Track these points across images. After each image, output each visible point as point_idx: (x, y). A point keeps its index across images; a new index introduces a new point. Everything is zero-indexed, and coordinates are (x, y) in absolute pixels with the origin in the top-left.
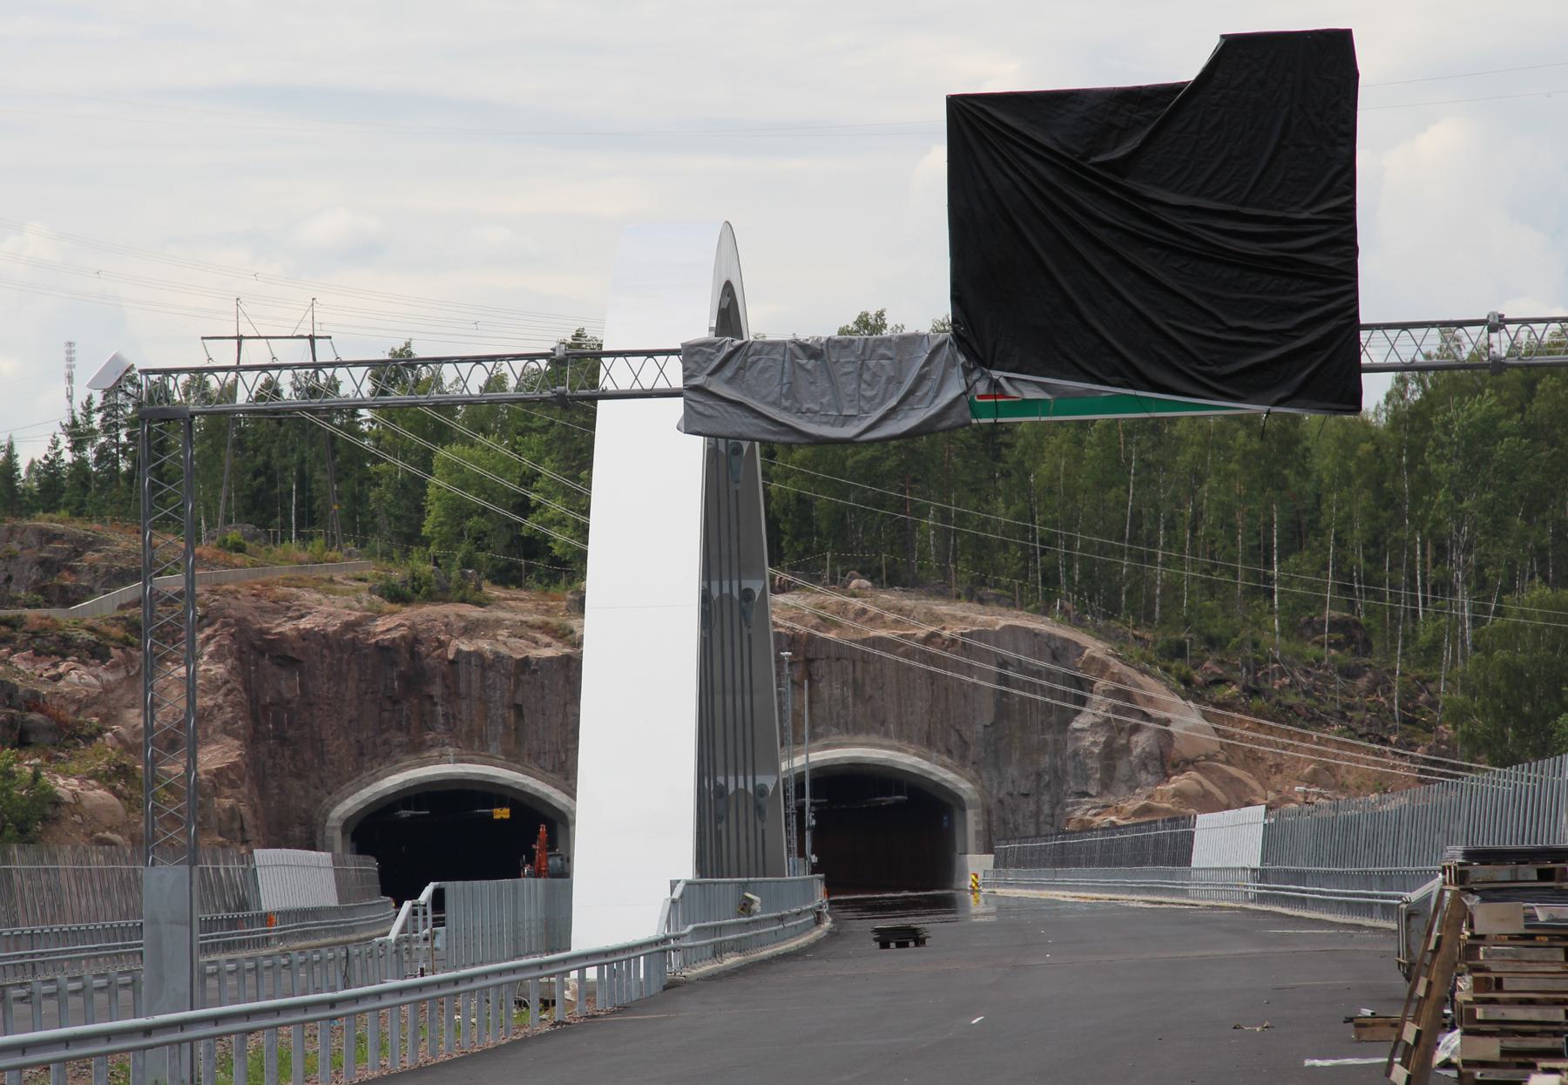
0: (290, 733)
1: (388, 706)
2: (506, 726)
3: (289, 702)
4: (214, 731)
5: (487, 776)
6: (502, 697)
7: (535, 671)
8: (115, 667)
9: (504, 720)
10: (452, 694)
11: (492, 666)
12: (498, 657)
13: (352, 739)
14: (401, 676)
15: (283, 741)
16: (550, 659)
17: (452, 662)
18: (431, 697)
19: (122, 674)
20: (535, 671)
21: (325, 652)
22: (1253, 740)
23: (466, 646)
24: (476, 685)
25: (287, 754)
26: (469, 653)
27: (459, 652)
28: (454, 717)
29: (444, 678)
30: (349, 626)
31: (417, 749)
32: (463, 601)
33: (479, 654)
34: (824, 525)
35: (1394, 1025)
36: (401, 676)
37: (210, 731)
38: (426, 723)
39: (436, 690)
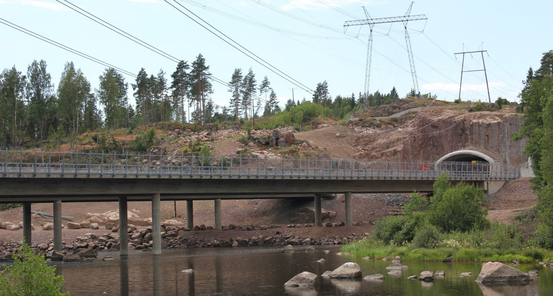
0: (436, 144)
2: (485, 141)
8: (382, 129)
10: (472, 133)
11: (481, 126)
14: (461, 129)
15: (434, 146)
17: (472, 125)
19: (384, 131)
22: (76, 123)
23: (475, 121)
29: (470, 129)
30: (451, 118)
31: (464, 147)
33: (478, 123)
34: (28, 80)
35: (117, 248)
36: (461, 129)
38: (466, 140)
39: (468, 132)
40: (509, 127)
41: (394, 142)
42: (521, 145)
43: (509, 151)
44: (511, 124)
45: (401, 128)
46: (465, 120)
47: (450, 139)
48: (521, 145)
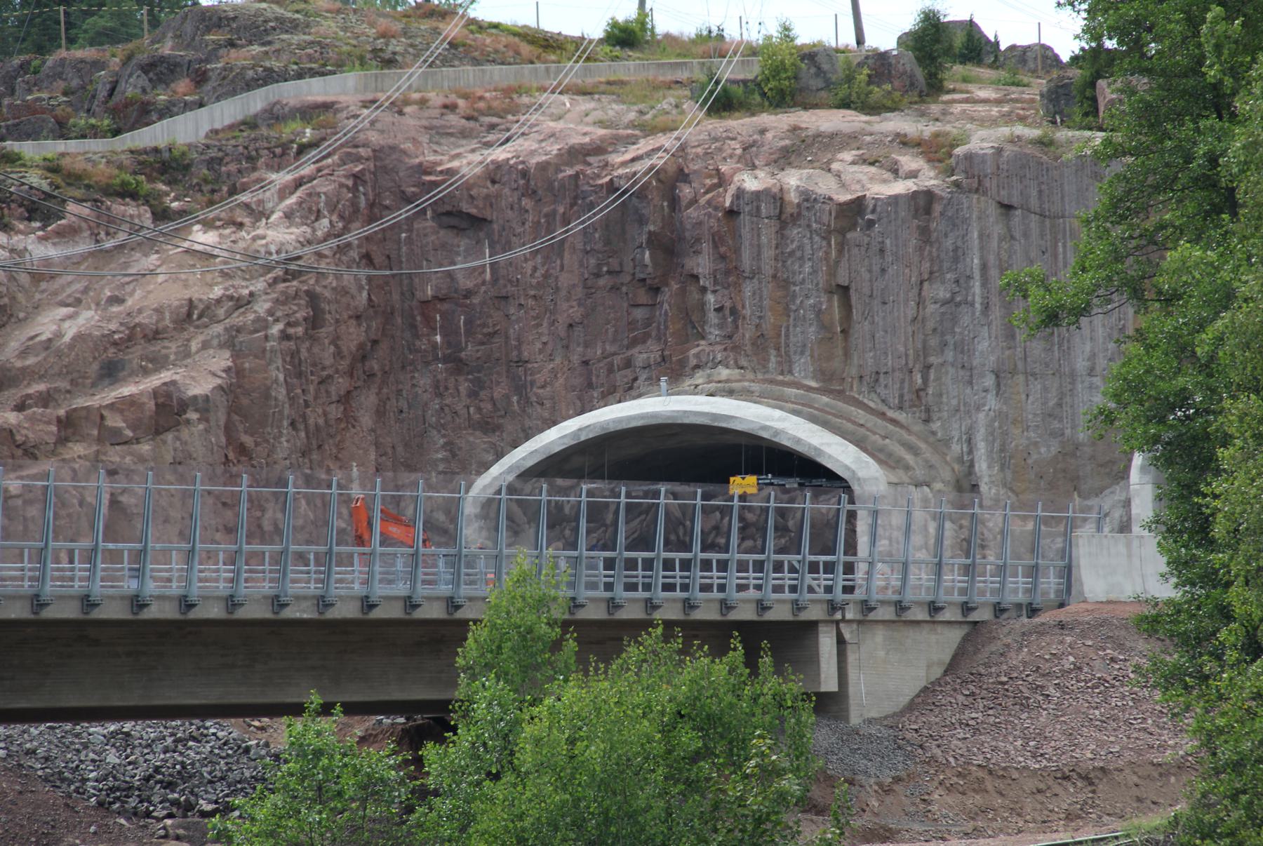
0: (470, 351)
1: (643, 297)
2: (824, 327)
3: (468, 294)
4: (205, 345)
5: (620, 420)
6: (814, 272)
7: (871, 224)
9: (819, 313)
10: (730, 273)
12: (808, 199)
13: (576, 359)
15: (458, 365)
16: (895, 199)
17: (732, 213)
18: (695, 277)
19: (83, 246)
20: (871, 224)
21: (527, 203)
23: (752, 182)
24: (768, 254)
25: (464, 387)
26: (757, 194)
27: (740, 193)
28: (734, 311)
29: (717, 240)
30: (577, 154)
31: (674, 371)
32: (845, 104)
33: (777, 198)
36: (654, 241)
37: (194, 346)
38: (692, 325)
39: (702, 264)
40: (997, 230)
41: (155, 335)
42: (1081, 364)
43: (992, 402)
44: (1007, 208)
45: (208, 225)
46: (682, 176)
47: (576, 312)
48: (1081, 364)
